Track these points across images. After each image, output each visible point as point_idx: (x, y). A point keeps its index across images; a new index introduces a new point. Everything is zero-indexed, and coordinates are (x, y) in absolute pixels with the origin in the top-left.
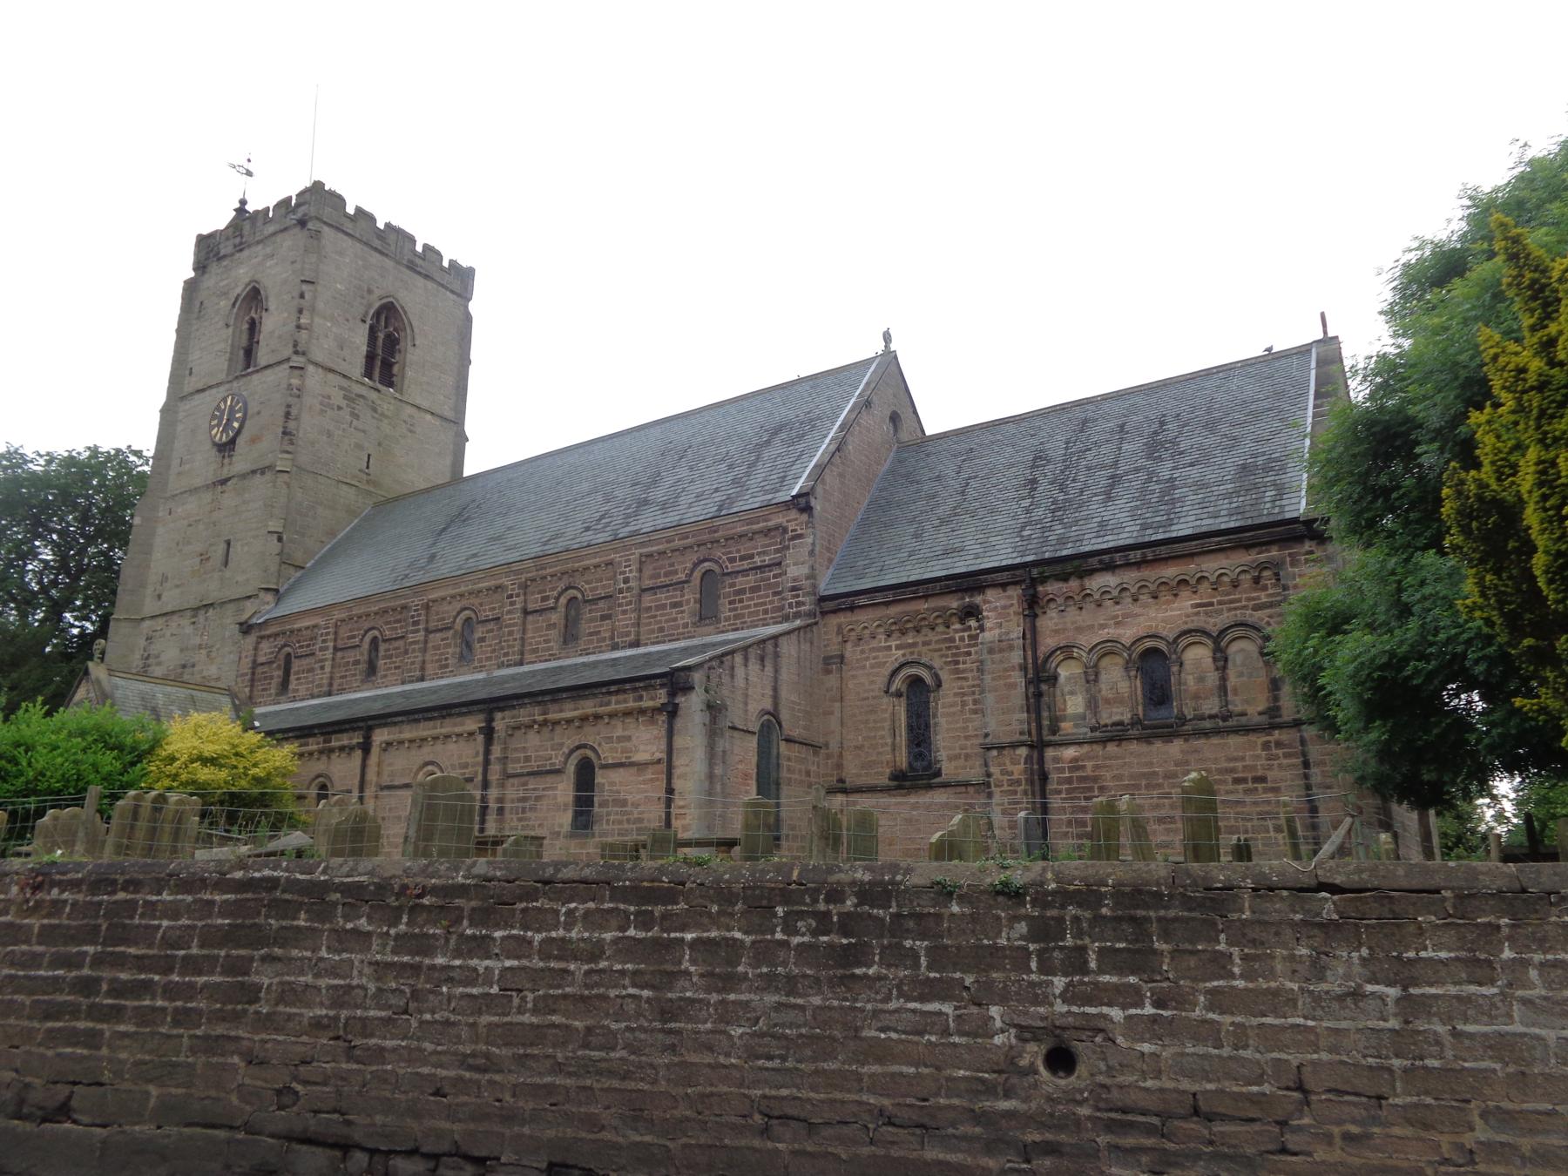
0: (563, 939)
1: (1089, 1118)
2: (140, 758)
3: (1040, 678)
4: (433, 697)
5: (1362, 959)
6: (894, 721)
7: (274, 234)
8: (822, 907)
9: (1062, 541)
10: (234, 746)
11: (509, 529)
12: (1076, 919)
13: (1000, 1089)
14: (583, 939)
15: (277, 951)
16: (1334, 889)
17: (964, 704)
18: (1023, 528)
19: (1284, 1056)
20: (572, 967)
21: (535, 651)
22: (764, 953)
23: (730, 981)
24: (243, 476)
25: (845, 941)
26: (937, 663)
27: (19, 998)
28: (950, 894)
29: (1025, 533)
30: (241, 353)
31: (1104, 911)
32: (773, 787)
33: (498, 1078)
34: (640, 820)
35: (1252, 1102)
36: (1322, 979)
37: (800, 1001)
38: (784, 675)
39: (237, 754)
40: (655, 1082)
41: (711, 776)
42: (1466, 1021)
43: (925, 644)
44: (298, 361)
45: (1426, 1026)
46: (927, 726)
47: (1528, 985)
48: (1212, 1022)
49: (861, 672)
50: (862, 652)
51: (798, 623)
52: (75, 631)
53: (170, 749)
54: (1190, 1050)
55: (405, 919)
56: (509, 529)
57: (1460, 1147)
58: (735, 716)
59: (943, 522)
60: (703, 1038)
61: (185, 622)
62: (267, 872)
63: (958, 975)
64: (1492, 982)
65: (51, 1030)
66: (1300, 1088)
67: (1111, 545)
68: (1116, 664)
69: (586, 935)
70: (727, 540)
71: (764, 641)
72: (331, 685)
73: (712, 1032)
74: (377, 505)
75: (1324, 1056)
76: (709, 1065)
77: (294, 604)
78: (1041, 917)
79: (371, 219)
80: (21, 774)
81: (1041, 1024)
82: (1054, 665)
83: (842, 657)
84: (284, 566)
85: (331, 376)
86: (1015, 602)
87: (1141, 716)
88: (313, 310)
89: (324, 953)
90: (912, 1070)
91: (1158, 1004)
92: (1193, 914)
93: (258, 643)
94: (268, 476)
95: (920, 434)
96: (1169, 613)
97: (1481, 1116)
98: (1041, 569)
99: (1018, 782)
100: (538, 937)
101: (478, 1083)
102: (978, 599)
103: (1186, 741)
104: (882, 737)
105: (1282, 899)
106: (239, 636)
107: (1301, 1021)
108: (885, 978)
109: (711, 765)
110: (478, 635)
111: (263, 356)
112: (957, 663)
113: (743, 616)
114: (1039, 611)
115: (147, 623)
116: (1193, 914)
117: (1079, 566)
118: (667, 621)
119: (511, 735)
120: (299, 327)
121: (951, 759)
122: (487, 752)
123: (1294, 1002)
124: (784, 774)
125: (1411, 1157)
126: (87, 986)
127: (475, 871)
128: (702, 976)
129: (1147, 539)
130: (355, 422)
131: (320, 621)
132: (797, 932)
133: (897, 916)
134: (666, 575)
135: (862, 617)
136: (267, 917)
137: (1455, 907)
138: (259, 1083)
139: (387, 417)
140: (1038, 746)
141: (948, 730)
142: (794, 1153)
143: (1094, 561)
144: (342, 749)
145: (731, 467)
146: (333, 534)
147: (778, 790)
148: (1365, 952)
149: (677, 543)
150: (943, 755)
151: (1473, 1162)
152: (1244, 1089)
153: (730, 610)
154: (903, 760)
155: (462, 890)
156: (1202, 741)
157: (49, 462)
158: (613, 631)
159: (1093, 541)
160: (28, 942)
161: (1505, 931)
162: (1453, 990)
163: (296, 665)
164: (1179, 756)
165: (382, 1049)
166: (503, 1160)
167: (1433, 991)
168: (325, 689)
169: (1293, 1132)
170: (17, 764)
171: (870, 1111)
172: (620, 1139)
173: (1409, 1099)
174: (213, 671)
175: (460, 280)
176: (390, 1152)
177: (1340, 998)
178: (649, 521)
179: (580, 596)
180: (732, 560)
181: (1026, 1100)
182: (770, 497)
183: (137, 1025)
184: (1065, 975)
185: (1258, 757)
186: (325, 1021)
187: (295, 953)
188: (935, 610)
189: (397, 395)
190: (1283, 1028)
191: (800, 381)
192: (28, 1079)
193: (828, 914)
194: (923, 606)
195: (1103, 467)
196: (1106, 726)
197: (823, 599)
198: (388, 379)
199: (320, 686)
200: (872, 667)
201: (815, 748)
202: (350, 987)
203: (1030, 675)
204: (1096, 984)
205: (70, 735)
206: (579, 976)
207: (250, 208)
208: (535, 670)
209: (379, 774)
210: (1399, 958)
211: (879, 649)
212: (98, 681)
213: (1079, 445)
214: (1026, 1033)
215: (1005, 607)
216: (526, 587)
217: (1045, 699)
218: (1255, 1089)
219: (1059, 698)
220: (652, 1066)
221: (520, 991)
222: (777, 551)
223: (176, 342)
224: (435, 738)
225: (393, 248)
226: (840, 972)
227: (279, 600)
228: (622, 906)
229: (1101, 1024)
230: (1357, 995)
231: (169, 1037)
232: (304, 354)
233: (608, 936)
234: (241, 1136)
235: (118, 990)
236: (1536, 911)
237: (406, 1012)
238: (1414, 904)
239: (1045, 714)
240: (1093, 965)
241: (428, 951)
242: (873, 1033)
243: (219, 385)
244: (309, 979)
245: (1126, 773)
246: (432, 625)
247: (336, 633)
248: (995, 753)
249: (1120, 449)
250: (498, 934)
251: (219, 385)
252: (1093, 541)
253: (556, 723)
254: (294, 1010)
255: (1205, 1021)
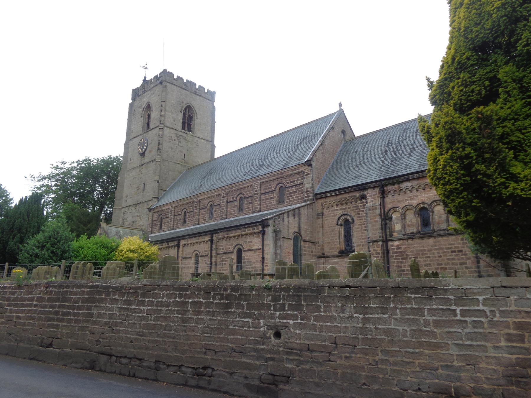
0: (161, 301)
1: (282, 351)
2: (113, 250)
3: (386, 219)
4: (198, 230)
5: (354, 307)
6: (339, 234)
7: (153, 87)
8: (222, 292)
9: (393, 172)
10: (140, 247)
11: (223, 176)
12: (283, 295)
13: (261, 343)
14: (166, 301)
15: (98, 304)
16: (350, 287)
17: (362, 228)
18: (381, 168)
19: (331, 334)
20: (163, 309)
21: (231, 214)
22: (208, 305)
23: (199, 313)
24: (148, 163)
25: (227, 302)
26: (353, 214)
27: (42, 316)
28: (253, 289)
29: (381, 169)
30: (146, 125)
31: (291, 293)
32: (299, 256)
33: (145, 338)
34: (255, 267)
35: (323, 347)
36: (343, 312)
37: (215, 318)
38: (302, 220)
39: (141, 249)
40: (180, 340)
41: (276, 253)
42: (379, 324)
43: (349, 208)
44: (161, 126)
45: (369, 326)
46: (350, 235)
47: (396, 314)
48: (315, 324)
49: (329, 218)
50: (329, 211)
51: (308, 202)
52: (108, 212)
53: (122, 247)
54: (308, 332)
55: (126, 296)
56: (223, 176)
57: (374, 360)
58: (284, 233)
59: (356, 167)
60: (192, 328)
61: (133, 208)
62: (97, 283)
63: (253, 311)
64: (387, 313)
65: (48, 324)
66: (335, 343)
67: (408, 172)
68: (411, 213)
69: (167, 300)
70: (286, 176)
71: (294, 209)
72: (173, 226)
73: (194, 326)
74: (187, 170)
75: (342, 334)
76: (193, 335)
77: (163, 202)
78: (275, 295)
79: (182, 79)
80: (80, 256)
81: (273, 325)
82: (391, 214)
83: (323, 214)
84: (160, 190)
85: (172, 130)
86: (377, 193)
87: (420, 230)
88: (165, 110)
89: (108, 305)
90: (241, 337)
91: (302, 319)
92: (313, 294)
93: (153, 214)
94: (154, 163)
95: (353, 137)
96: (429, 195)
97: (381, 352)
98: (385, 182)
99: (379, 253)
100: (156, 301)
101: (140, 339)
102: (365, 193)
103: (435, 238)
104: (336, 239)
105: (336, 290)
106: (148, 212)
107: (337, 324)
108: (236, 312)
109: (276, 249)
110: (214, 210)
111: (152, 126)
112: (359, 214)
113: (292, 201)
114: (385, 196)
115: (123, 209)
116: (313, 294)
117: (398, 180)
118: (269, 204)
119: (218, 241)
120: (161, 116)
121: (358, 246)
122: (212, 247)
123: (336, 319)
124: (303, 252)
125: (361, 363)
126: (57, 313)
127: (143, 283)
128: (193, 311)
129: (421, 170)
130: (180, 144)
131: (170, 207)
132: (215, 299)
133: (240, 295)
134: (269, 188)
135: (329, 200)
136: (96, 295)
137: (380, 292)
138: (93, 339)
139: (190, 142)
140: (385, 241)
141: (357, 236)
142: (212, 359)
143: (403, 178)
144: (172, 246)
145: (289, 152)
146: (175, 180)
147: (301, 257)
148: (355, 305)
149: (271, 178)
150: (355, 245)
151: (377, 365)
152: (321, 343)
153: (288, 199)
154: (343, 246)
155: (139, 288)
156: (440, 238)
157: (98, 161)
158: (253, 207)
159: (403, 171)
160: (44, 302)
161: (392, 299)
162: (376, 316)
163: (164, 221)
164: (433, 244)
165: (120, 330)
166: (145, 359)
167: (371, 316)
168: (172, 228)
169: (332, 355)
170: (79, 253)
171: (230, 348)
172: (172, 355)
173: (362, 347)
174: (141, 223)
175: (210, 96)
176: (120, 357)
177: (348, 318)
178: (263, 171)
179: (243, 196)
180: (288, 183)
181: (268, 345)
182: (299, 162)
183: (67, 323)
184: (279, 311)
185: (459, 243)
186: (107, 323)
187: (102, 305)
188: (352, 197)
189: (193, 134)
190: (332, 326)
191: (313, 122)
192: (44, 337)
193: (223, 294)
194: (348, 195)
195: (410, 145)
196: (408, 234)
197: (316, 194)
198: (190, 130)
199: (170, 227)
200: (333, 216)
201: (314, 243)
202: (113, 314)
203: (383, 218)
204: (287, 314)
205: (94, 244)
206: (164, 311)
207: (147, 79)
208: (223, 222)
209: (182, 254)
210: (363, 307)
211: (334, 210)
212: (103, 228)
213: (403, 138)
214: (269, 327)
215: (374, 195)
216: (227, 194)
217: (388, 225)
218: (324, 343)
219: (393, 225)
220: (180, 335)
221: (151, 315)
222: (302, 179)
223: (128, 123)
224: (197, 243)
225: (189, 88)
226: (225, 310)
227: (158, 201)
228: (175, 292)
229: (287, 325)
230: (351, 317)
231: (73, 326)
232: (163, 124)
233: (171, 300)
234: (88, 352)
235: (64, 314)
236: (401, 293)
237: (125, 321)
238: (369, 291)
239: (388, 230)
240: (286, 309)
241: (130, 304)
242: (232, 327)
243: (140, 135)
244: (104, 312)
245: (415, 250)
246: (201, 207)
247: (174, 211)
248: (371, 244)
249: (416, 138)
250: (147, 300)
251: (140, 135)
252: (403, 171)
253: (231, 237)
254: (101, 320)
255: (313, 324)
